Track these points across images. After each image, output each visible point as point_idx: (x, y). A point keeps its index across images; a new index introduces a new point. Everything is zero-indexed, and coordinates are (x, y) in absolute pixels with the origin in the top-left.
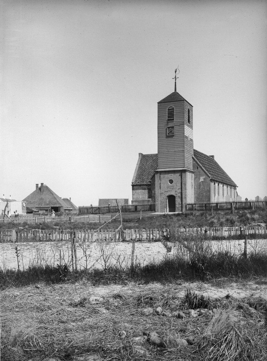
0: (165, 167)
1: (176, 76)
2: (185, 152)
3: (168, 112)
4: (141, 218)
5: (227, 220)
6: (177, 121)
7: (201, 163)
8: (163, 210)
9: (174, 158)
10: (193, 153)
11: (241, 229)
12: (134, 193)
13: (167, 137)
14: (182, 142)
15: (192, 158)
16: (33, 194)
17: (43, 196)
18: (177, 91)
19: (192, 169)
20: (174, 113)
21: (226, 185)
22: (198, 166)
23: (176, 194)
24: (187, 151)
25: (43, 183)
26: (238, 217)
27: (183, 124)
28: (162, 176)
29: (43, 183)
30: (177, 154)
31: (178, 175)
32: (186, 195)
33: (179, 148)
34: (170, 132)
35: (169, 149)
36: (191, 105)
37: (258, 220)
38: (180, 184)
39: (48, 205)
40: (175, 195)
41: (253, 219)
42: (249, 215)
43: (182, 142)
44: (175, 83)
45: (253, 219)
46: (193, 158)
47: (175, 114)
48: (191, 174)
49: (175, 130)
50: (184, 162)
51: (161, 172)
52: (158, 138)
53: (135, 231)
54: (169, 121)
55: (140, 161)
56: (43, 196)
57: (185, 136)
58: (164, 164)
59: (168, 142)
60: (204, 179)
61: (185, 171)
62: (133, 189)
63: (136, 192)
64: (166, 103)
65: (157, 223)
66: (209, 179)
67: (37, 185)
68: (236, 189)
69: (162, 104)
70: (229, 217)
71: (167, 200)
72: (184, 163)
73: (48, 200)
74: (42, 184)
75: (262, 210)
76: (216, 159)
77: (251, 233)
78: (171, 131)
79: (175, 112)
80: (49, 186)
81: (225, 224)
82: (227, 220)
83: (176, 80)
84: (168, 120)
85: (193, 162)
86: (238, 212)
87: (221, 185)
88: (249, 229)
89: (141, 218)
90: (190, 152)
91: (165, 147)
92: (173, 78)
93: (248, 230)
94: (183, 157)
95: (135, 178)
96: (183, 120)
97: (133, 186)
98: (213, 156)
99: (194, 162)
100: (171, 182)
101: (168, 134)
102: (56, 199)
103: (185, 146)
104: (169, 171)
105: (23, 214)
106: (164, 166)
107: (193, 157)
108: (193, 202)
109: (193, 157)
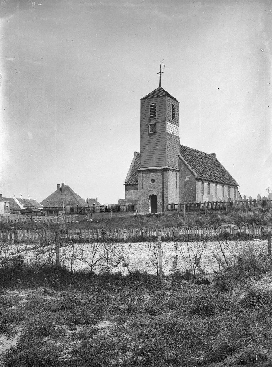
0: (147, 166)
1: (160, 71)
2: (167, 150)
3: (151, 108)
4: (111, 219)
5: (197, 221)
6: (160, 117)
7: (186, 160)
8: (144, 210)
9: (156, 156)
10: (179, 151)
11: (141, 231)
12: (127, 193)
13: (150, 134)
14: (164, 140)
15: (177, 157)
16: (54, 194)
17: (63, 197)
18: (162, 87)
19: (177, 167)
20: (156, 109)
21: (222, 185)
22: (184, 165)
23: (158, 194)
24: (170, 149)
25: (64, 184)
26: (210, 218)
27: (165, 121)
28: (144, 175)
29: (64, 184)
30: (159, 152)
31: (159, 174)
32: (167, 195)
33: (161, 146)
34: (152, 129)
35: (151, 147)
36: (178, 101)
37: (229, 221)
38: (161, 183)
39: (68, 205)
40: (156, 195)
41: (224, 221)
42: (219, 217)
43: (164, 140)
44: (160, 78)
45: (224, 221)
46: (179, 156)
47: (157, 110)
48: (175, 173)
49: (158, 127)
50: (166, 160)
51: (143, 171)
52: (141, 135)
53: (28, 232)
54: (152, 118)
55: (135, 160)
56: (63, 197)
57: (167, 133)
58: (146, 162)
59: (151, 139)
60: (189, 178)
61: (166, 170)
62: (126, 189)
63: (128, 192)
64: (149, 100)
65: (126, 224)
66: (195, 178)
67: (58, 185)
68: (237, 189)
69: (144, 100)
70: (200, 218)
71: (149, 200)
72: (165, 161)
73: (68, 200)
74: (63, 184)
75: (235, 211)
76: (217, 157)
77: (151, 235)
78: (153, 129)
79: (157, 108)
80: (69, 187)
81: (193, 225)
82: (197, 221)
83: (160, 75)
84: (151, 117)
85: (179, 160)
86: (211, 213)
87: (213, 185)
88: (150, 231)
89: (111, 219)
90: (175, 150)
91: (147, 145)
92: (158, 74)
93: (149, 232)
94: (165, 155)
95: (128, 178)
96: (165, 117)
97: (126, 185)
98: (214, 154)
99: (180, 161)
100: (153, 181)
101: (151, 131)
102: (76, 199)
103: (167, 144)
104: (150, 170)
105: (6, 214)
106: (147, 164)
107: (179, 154)
108: (179, 202)
109: (179, 154)
